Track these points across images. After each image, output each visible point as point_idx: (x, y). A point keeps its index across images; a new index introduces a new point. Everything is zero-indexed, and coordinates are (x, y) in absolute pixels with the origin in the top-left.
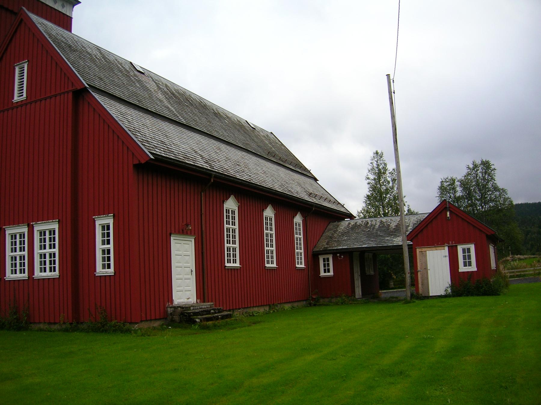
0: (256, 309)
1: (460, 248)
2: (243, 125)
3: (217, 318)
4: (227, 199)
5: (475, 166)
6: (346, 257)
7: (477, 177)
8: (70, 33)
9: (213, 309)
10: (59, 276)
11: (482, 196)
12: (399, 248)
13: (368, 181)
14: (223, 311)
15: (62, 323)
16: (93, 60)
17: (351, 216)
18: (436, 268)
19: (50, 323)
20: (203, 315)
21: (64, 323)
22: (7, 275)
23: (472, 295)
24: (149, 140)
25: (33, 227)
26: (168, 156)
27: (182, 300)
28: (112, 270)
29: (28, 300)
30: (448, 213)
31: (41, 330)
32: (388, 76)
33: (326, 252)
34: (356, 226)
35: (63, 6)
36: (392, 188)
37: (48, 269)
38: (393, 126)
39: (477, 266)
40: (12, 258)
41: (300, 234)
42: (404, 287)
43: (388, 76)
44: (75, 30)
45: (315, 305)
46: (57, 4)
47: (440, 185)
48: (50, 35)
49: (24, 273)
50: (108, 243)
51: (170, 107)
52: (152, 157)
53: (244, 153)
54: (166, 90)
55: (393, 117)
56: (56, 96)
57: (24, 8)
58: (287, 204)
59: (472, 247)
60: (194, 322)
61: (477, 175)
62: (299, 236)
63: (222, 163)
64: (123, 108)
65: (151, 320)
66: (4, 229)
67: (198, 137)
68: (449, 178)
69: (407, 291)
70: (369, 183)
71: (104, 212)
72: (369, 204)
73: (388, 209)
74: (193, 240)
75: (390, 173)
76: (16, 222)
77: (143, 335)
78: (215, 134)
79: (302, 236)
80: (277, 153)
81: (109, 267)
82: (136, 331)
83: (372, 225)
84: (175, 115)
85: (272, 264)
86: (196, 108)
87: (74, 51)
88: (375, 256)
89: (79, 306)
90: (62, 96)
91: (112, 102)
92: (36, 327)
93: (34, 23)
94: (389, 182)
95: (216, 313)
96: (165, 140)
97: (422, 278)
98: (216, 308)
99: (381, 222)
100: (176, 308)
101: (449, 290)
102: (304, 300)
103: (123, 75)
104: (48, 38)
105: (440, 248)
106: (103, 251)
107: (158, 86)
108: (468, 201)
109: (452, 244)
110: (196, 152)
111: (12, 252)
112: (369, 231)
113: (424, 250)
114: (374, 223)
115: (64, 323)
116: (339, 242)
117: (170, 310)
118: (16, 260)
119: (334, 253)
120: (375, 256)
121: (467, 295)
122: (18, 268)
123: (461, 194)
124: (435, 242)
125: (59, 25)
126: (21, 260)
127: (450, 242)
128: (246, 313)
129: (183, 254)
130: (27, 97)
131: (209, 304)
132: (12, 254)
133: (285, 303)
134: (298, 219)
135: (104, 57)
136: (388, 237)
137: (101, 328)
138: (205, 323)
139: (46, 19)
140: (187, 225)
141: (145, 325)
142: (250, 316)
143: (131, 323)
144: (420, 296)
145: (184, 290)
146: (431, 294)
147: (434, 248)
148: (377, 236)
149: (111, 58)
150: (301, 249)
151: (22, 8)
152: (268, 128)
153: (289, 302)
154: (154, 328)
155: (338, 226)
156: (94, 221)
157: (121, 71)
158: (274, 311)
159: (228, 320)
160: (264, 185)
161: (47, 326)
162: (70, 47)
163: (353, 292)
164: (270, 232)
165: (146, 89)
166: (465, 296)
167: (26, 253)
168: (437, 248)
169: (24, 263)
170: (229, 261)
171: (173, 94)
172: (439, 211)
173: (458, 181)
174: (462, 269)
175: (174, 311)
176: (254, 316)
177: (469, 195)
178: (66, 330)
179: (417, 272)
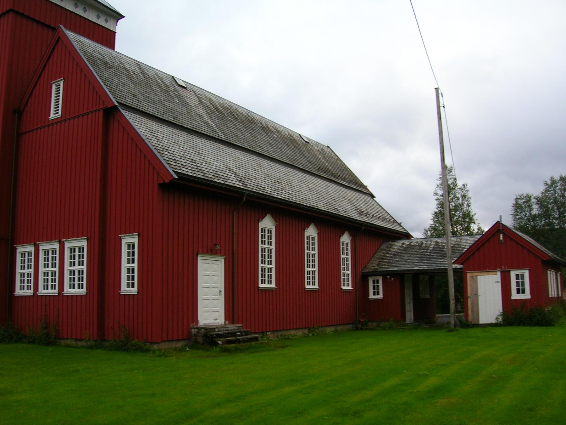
0: (293, 332)
1: (513, 274)
2: (294, 139)
3: (239, 342)
4: (263, 218)
5: (554, 182)
6: (397, 280)
7: (555, 194)
8: (105, 50)
9: (239, 332)
10: (87, 293)
12: (445, 271)
13: (436, 197)
14: (251, 333)
16: (129, 77)
17: (408, 236)
18: (488, 294)
19: (77, 340)
20: (228, 337)
21: (89, 340)
23: (524, 325)
24: (177, 159)
25: (64, 244)
26: (195, 175)
27: (208, 321)
28: (84, 290)
29: (58, 316)
30: (501, 236)
31: (68, 346)
32: (437, 89)
33: (375, 273)
35: (107, 21)
36: (462, 205)
37: (76, 286)
38: (440, 143)
39: (532, 293)
40: (71, 272)
41: (347, 254)
43: (437, 89)
44: (120, 46)
45: (361, 329)
47: (514, 202)
48: (85, 53)
49: (82, 288)
50: (133, 262)
51: (210, 122)
52: (176, 177)
53: (290, 170)
54: (208, 104)
55: (441, 133)
56: (88, 114)
57: (61, 26)
58: (331, 224)
59: (526, 273)
60: (216, 344)
61: (555, 192)
62: (346, 256)
63: (259, 181)
64: (154, 126)
66: (63, 242)
67: (237, 153)
68: (525, 194)
69: (451, 318)
70: (437, 199)
71: (129, 231)
72: (437, 222)
73: (456, 228)
74: (223, 260)
75: (460, 189)
76: (48, 239)
77: (160, 356)
78: (258, 150)
80: (330, 168)
81: (133, 286)
82: (154, 351)
83: (426, 246)
84: (214, 131)
85: (313, 285)
86: (242, 122)
87: (110, 68)
88: (431, 279)
89: (102, 323)
90: (94, 114)
91: (144, 120)
92: (63, 342)
93: (70, 41)
94: (458, 199)
95: (242, 335)
96: (197, 158)
97: (472, 304)
98: (243, 330)
99: (437, 243)
100: (199, 329)
101: (500, 318)
104: (82, 56)
106: (128, 269)
107: (200, 101)
109: (505, 269)
110: (230, 170)
111: (71, 266)
112: (422, 252)
113: (475, 274)
114: (429, 243)
115: (89, 340)
116: (390, 264)
117: (194, 331)
119: (385, 275)
120: (431, 279)
121: (519, 325)
123: (537, 212)
124: (487, 267)
125: (98, 41)
126: (79, 274)
128: (281, 335)
129: (211, 275)
130: (62, 115)
131: (236, 325)
133: (327, 326)
134: (346, 239)
135: (143, 72)
136: (441, 259)
137: (124, 347)
138: (226, 345)
140: (216, 245)
141: (164, 346)
142: (286, 339)
143: (152, 343)
144: (468, 324)
145: (211, 310)
146: (481, 323)
147: (485, 273)
148: (430, 258)
149: (151, 74)
150: (348, 270)
152: (325, 142)
153: (332, 325)
154: (175, 349)
155: (391, 246)
158: (313, 335)
159: (253, 343)
160: (305, 203)
161: (74, 343)
162: (106, 63)
164: (312, 252)
165: (185, 104)
167: (57, 269)
168: (489, 273)
169: (83, 278)
170: (263, 282)
171: (216, 108)
172: (492, 234)
173: (534, 198)
174: (515, 296)
175: (198, 332)
176: (289, 338)
177: (546, 214)
178: (91, 347)
179: (467, 298)
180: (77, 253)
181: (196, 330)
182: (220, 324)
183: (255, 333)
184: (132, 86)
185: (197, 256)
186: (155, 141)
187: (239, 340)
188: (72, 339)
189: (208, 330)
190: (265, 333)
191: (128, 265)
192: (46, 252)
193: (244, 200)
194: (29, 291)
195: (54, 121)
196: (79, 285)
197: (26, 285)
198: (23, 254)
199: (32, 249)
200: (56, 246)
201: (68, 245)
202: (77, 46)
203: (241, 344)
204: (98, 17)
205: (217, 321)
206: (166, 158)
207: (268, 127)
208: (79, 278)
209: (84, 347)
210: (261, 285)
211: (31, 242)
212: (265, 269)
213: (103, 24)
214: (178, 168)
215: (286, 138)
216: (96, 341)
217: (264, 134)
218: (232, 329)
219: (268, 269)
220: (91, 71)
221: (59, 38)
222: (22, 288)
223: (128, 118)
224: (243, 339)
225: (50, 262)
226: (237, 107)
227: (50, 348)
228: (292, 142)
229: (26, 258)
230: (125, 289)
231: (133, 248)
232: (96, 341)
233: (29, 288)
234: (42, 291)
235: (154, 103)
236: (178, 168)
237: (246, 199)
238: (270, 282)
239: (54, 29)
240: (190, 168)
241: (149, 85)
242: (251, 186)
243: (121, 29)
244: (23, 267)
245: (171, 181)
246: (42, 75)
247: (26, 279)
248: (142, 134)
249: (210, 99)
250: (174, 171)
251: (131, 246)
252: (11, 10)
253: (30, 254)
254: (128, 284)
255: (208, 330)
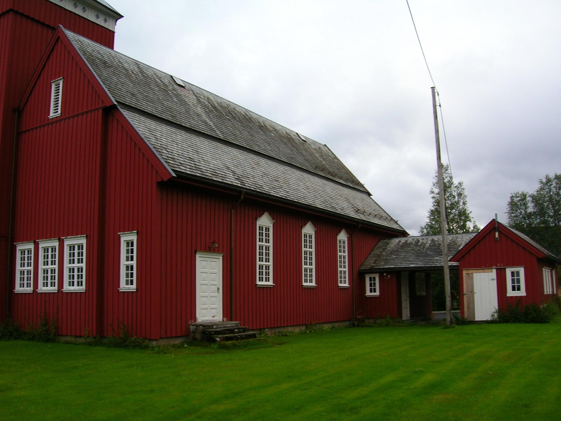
0: (290, 329)
1: (508, 271)
2: (291, 138)
3: (237, 338)
4: (260, 216)
5: (549, 181)
6: (393, 277)
7: (550, 192)
8: (104, 49)
9: (237, 329)
10: (86, 290)
11: (555, 212)
12: (441, 269)
13: (432, 195)
14: (249, 330)
15: (86, 336)
16: (128, 75)
17: (404, 234)
18: (483, 291)
19: (76, 336)
20: (225, 334)
21: (88, 337)
22: (39, 288)
23: (519, 322)
24: (175, 157)
25: (63, 242)
26: (193, 173)
27: (206, 318)
29: (57, 313)
30: (497, 234)
31: (67, 343)
32: (433, 88)
33: (372, 271)
34: (406, 244)
35: (106, 21)
36: (458, 203)
38: (436, 142)
40: (70, 269)
41: (344, 252)
42: (444, 309)
43: (433, 88)
44: (119, 46)
45: (358, 326)
46: (99, 19)
47: (510, 200)
48: (85, 53)
49: (82, 285)
50: (132, 260)
51: (208, 121)
53: (287, 168)
54: (207, 103)
55: (437, 131)
57: (61, 26)
58: (328, 221)
59: (522, 270)
60: (215, 341)
61: (550, 190)
62: (343, 254)
63: (257, 179)
64: (153, 124)
65: (172, 337)
66: (63, 239)
67: (235, 152)
68: (520, 193)
69: (447, 315)
70: (433, 198)
71: (128, 229)
72: (433, 220)
73: (452, 225)
74: (221, 258)
75: (456, 187)
76: (48, 236)
77: (158, 352)
78: (256, 149)
79: (346, 254)
80: (327, 166)
81: (132, 284)
82: (153, 348)
83: (423, 243)
84: (212, 130)
85: (310, 283)
86: (240, 121)
87: (109, 67)
88: (428, 276)
89: (101, 320)
91: (143, 118)
92: (63, 339)
94: (454, 197)
95: (240, 332)
96: (195, 157)
97: (467, 301)
99: (433, 240)
100: (198, 326)
101: (496, 315)
102: (347, 321)
103: (160, 89)
104: (82, 55)
105: (488, 270)
106: (127, 267)
107: (198, 100)
108: (541, 218)
109: (501, 266)
110: (228, 168)
111: (70, 263)
113: (471, 272)
114: (425, 241)
115: (88, 337)
116: (386, 261)
117: (192, 328)
118: (73, 272)
119: (381, 272)
120: (428, 276)
121: (514, 322)
122: (76, 280)
123: (532, 210)
124: (482, 264)
125: (97, 41)
126: (78, 272)
127: (499, 265)
128: (279, 332)
129: (209, 272)
130: (61, 113)
131: (234, 322)
132: (44, 267)
133: (324, 323)
134: (343, 236)
135: (142, 72)
136: (437, 256)
137: (123, 344)
138: (224, 342)
139: (83, 35)
140: (214, 243)
141: (163, 342)
142: (283, 335)
143: (150, 340)
144: (464, 321)
145: (209, 307)
146: (476, 320)
147: (481, 271)
148: (427, 255)
149: (150, 73)
150: (345, 267)
151: (59, 26)
153: (329, 322)
154: (174, 346)
155: (388, 244)
156: (120, 238)
157: (158, 86)
158: (310, 331)
160: (303, 201)
161: (73, 339)
162: (105, 63)
163: (400, 313)
164: (309, 250)
165: (183, 103)
166: (511, 323)
167: (56, 267)
169: (82, 275)
170: (261, 279)
171: (214, 107)
172: (488, 232)
173: (530, 196)
174: (510, 293)
175: (196, 329)
176: (286, 335)
177: (541, 212)
178: (90, 344)
179: (463, 295)
180: (76, 251)
181: (194, 327)
182: (218, 320)
183: (253, 330)
184: (131, 85)
185: (196, 253)
186: (153, 140)
187: (237, 336)
188: (71, 336)
189: (206, 327)
190: (262, 330)
191: (127, 262)
192: (46, 250)
193: (242, 198)
194: (29, 288)
195: (54, 120)
196: (78, 282)
197: (25, 282)
198: (23, 252)
199: (31, 246)
200: (56, 244)
201: (68, 242)
202: (76, 46)
203: (239, 341)
204: (98, 17)
205: (215, 318)
206: (164, 157)
207: (266, 126)
208: (78, 275)
209: (83, 344)
210: (258, 283)
211: (31, 240)
212: (262, 266)
213: (102, 24)
214: (176, 166)
215: (283, 137)
216: (95, 338)
217: (262, 133)
218: (230, 325)
219: (266, 267)
220: (90, 70)
221: (59, 37)
222: (22, 285)
223: (127, 117)
224: (241, 336)
225: (50, 260)
226: (235, 106)
227: (50, 345)
228: (289, 141)
229: (26, 256)
230: (124, 286)
231: (132, 246)
232: (95, 338)
233: (28, 285)
234: (42, 289)
235: (152, 102)
236: (176, 166)
237: (244, 197)
238: (267, 280)
239: (53, 29)
240: (188, 167)
241: (147, 84)
242: (249, 184)
243: (120, 29)
244: (23, 265)
245: (169, 179)
246: (42, 75)
247: (26, 276)
248: (140, 133)
249: (208, 98)
250: (172, 170)
251: (130, 244)
252: (11, 10)
253: (29, 251)
254: (127, 281)
255: (206, 327)
